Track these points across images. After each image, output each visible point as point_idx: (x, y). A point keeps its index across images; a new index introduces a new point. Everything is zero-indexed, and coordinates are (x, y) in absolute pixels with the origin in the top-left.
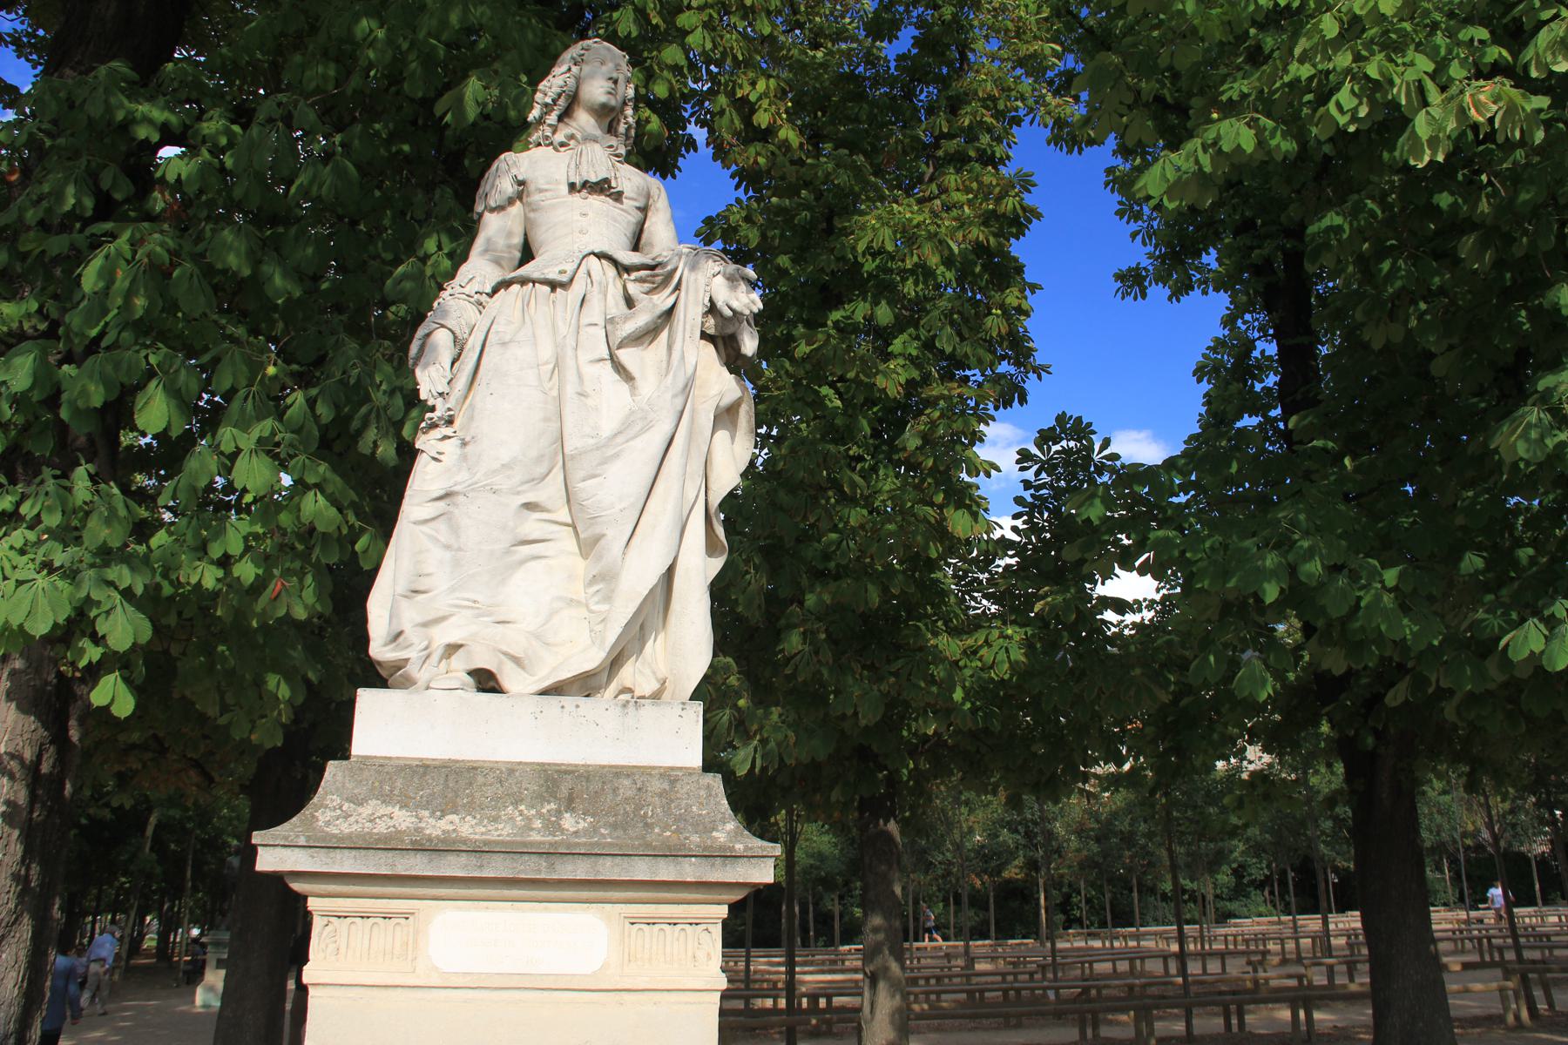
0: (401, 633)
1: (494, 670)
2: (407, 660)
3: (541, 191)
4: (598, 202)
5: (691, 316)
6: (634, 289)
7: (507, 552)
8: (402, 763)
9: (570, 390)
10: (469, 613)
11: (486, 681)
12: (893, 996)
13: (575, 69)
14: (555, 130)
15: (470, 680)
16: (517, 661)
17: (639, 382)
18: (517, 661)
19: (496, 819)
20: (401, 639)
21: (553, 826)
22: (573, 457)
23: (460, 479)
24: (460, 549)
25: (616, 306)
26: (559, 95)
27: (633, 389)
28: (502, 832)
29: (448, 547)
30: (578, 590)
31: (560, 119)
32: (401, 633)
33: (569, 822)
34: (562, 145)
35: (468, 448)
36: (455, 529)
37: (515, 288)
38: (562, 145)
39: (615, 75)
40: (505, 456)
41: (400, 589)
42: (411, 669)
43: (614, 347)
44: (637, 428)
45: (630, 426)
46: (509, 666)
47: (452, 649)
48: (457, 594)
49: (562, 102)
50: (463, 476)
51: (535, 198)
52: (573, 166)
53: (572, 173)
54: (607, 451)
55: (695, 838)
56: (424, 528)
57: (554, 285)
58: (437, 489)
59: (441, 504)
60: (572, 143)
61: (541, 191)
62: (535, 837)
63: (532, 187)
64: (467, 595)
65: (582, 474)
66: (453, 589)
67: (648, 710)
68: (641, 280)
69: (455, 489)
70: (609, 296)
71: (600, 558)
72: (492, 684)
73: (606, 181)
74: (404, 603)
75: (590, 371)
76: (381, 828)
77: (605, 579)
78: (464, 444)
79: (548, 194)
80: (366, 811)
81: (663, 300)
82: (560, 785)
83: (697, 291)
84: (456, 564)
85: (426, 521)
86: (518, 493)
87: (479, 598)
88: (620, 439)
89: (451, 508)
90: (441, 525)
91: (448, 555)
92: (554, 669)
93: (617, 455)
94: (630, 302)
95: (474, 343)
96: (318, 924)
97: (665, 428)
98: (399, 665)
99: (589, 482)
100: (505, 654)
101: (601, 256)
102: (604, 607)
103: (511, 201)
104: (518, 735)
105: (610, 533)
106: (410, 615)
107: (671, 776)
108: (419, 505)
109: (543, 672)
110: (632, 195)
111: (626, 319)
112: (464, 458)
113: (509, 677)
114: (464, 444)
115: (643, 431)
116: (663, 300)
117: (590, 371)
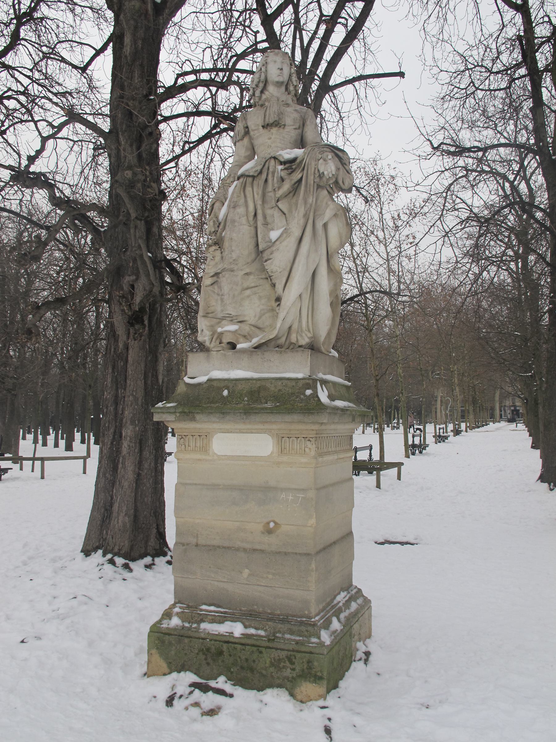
4: (274, 130)
10: (229, 319)
17: (287, 215)
24: (222, 295)
26: (259, 82)
29: (218, 295)
36: (220, 288)
48: (224, 312)
49: (261, 85)
50: (221, 266)
51: (252, 133)
57: (254, 177)
59: (215, 278)
64: (227, 312)
66: (222, 311)
75: (269, 212)
79: (256, 132)
81: (297, 176)
83: (311, 168)
84: (222, 300)
86: (242, 270)
90: (216, 287)
116: (297, 176)
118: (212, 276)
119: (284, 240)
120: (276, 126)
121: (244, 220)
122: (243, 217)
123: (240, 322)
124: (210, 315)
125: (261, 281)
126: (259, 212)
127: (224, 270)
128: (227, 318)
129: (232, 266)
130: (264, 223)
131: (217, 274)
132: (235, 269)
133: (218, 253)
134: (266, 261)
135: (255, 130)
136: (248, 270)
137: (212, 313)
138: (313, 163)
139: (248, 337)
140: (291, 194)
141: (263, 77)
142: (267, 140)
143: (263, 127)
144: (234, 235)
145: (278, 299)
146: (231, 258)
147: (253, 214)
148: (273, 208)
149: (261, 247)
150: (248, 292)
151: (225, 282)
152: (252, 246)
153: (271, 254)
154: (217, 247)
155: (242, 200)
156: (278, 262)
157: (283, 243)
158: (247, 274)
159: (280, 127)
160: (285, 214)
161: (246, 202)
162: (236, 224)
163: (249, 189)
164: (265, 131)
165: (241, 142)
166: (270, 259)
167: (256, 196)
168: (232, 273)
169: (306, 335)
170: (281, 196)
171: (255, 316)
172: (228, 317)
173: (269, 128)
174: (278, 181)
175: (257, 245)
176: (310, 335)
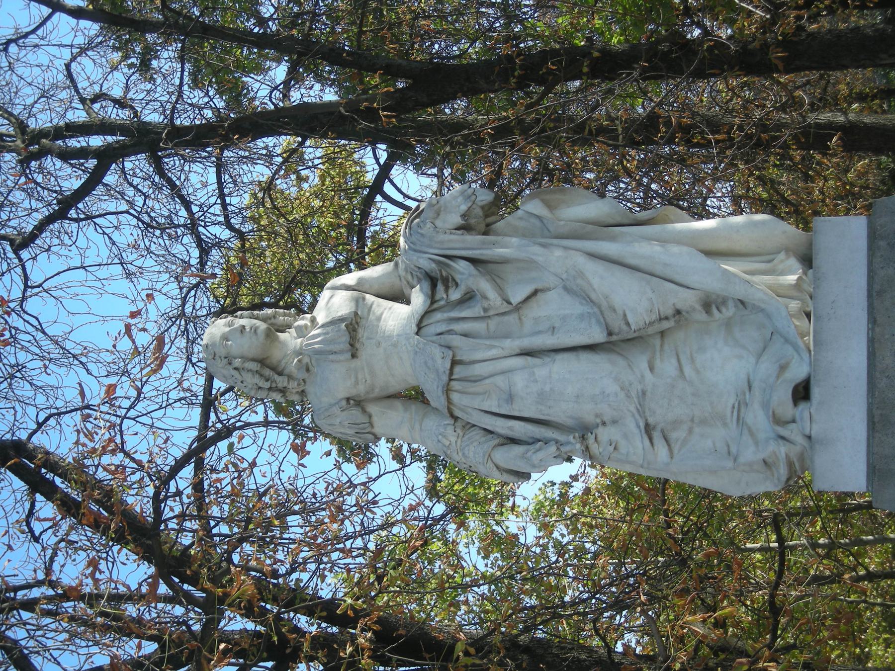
0: (765, 462)
1: (793, 385)
2: (787, 455)
5: (472, 244)
10: (743, 410)
11: (802, 392)
12: (571, 417)
14: (290, 377)
17: (539, 286)
18: (783, 368)
20: (770, 461)
22: (610, 334)
23: (632, 426)
24: (692, 420)
26: (261, 375)
29: (690, 431)
31: (280, 374)
32: (765, 462)
36: (676, 423)
37: (455, 397)
38: (308, 370)
42: (794, 451)
43: (509, 308)
48: (728, 421)
49: (267, 372)
56: (675, 451)
57: (454, 363)
58: (639, 443)
59: (656, 435)
61: (357, 383)
63: (353, 392)
65: (625, 327)
66: (725, 425)
69: (642, 425)
72: (801, 389)
74: (742, 460)
79: (360, 376)
83: (450, 241)
84: (703, 422)
86: (643, 376)
87: (730, 405)
88: (593, 296)
89: (659, 428)
90: (673, 435)
91: (697, 430)
94: (469, 298)
95: (502, 426)
97: (581, 261)
98: (790, 465)
100: (778, 377)
102: (731, 304)
103: (364, 411)
106: (750, 454)
107: (873, 236)
111: (485, 297)
112: (614, 422)
115: (581, 274)
117: (528, 325)
118: (651, 439)
119: (590, 285)
120: (355, 330)
122: (534, 373)
123: (750, 387)
124: (734, 450)
125: (666, 347)
127: (641, 411)
128: (742, 415)
129: (633, 394)
130: (550, 333)
131: (648, 430)
132: (639, 388)
133: (602, 432)
134: (628, 324)
135: (357, 378)
136: (644, 365)
137: (728, 446)
138: (442, 237)
139: (783, 361)
140: (498, 281)
141: (254, 366)
143: (354, 356)
145: (709, 304)
146: (616, 394)
147: (529, 358)
148: (520, 319)
149: (598, 336)
150: (688, 370)
153: (614, 310)
154: (591, 439)
155: (500, 381)
156: (633, 301)
157: (596, 286)
158: (652, 369)
159: (357, 323)
160: (535, 293)
161: (503, 372)
162: (547, 388)
163: (479, 370)
164: (363, 354)
165: (375, 419)
166: (625, 315)
167: (493, 353)
168: (648, 394)
169: (782, 261)
170: (500, 295)
171: (740, 357)
172: (739, 411)
173: (357, 345)
174: (469, 307)
175: (591, 348)
176: (782, 256)
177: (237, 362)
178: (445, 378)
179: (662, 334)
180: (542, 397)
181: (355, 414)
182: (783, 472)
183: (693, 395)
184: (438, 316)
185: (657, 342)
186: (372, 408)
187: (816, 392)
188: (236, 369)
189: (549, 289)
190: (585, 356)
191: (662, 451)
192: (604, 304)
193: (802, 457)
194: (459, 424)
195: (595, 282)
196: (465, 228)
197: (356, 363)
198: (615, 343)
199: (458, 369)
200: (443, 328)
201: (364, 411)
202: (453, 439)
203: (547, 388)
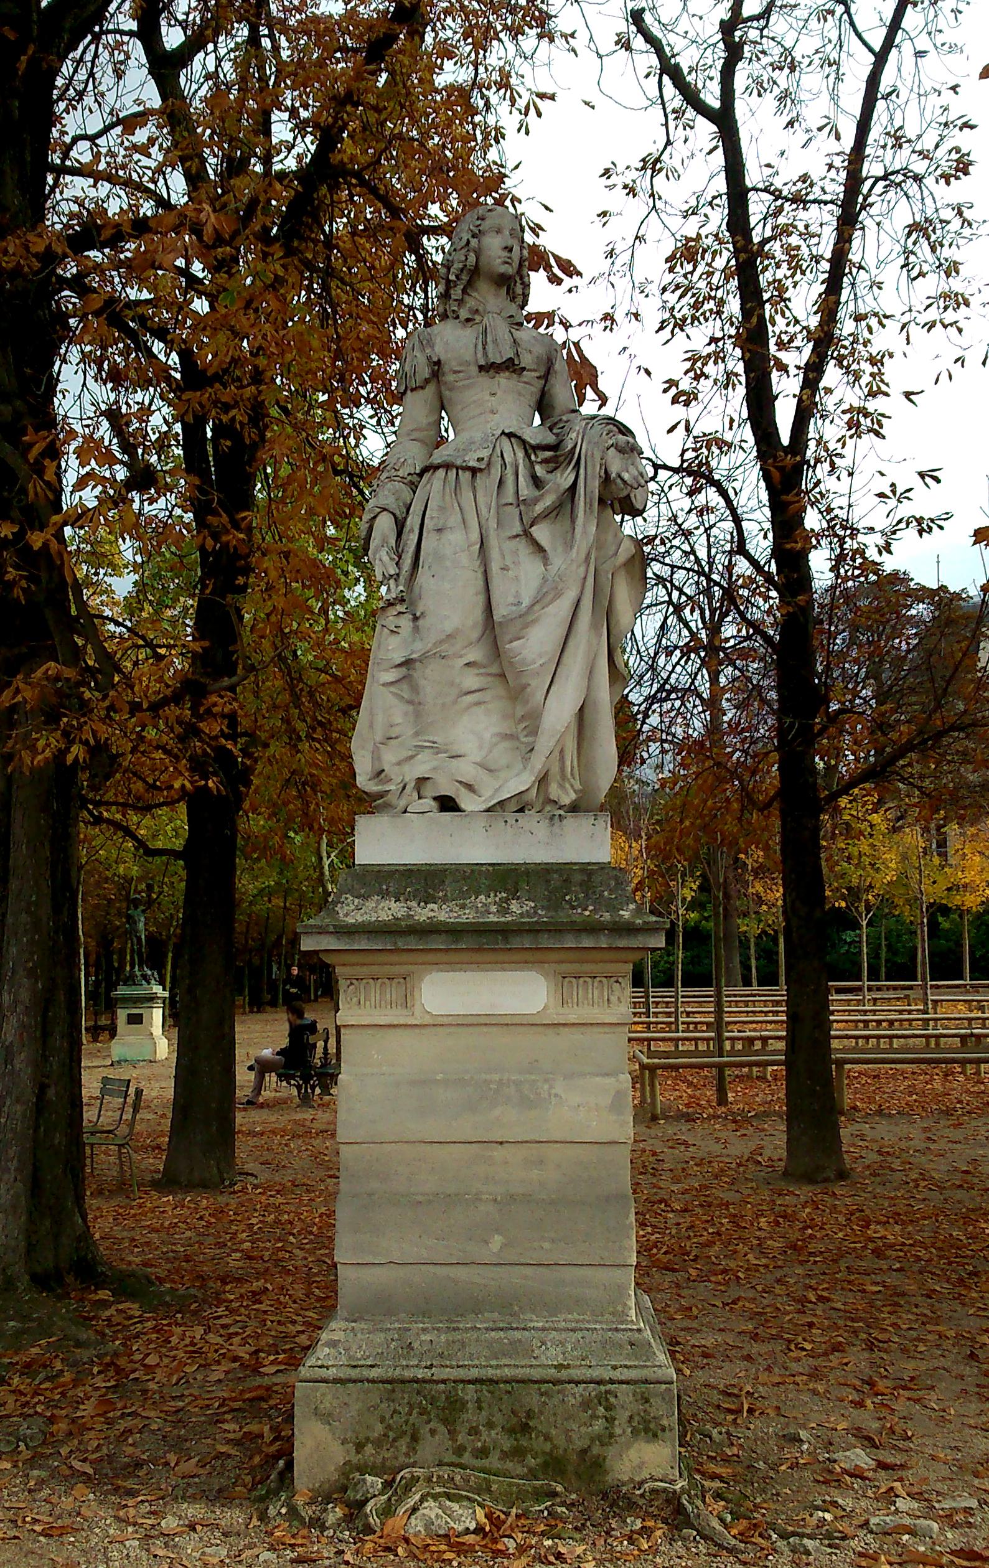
3: (455, 372)
4: (503, 380)
6: (539, 470)
7: (455, 702)
8: (377, 869)
9: (495, 567)
11: (447, 804)
13: (474, 242)
14: (460, 302)
15: (433, 803)
16: (470, 787)
18: (470, 787)
19: (463, 907)
21: (504, 911)
23: (418, 648)
25: (526, 490)
26: (462, 270)
27: (546, 561)
28: (468, 916)
29: (410, 702)
30: (506, 727)
31: (464, 291)
33: (514, 906)
34: (468, 320)
35: (420, 622)
36: (415, 689)
37: (441, 472)
39: (509, 244)
40: (449, 627)
41: (379, 737)
42: (391, 798)
44: (550, 596)
45: (545, 596)
46: (463, 790)
47: (421, 781)
49: (465, 277)
51: (450, 378)
52: (480, 347)
53: (480, 355)
54: (526, 618)
55: (607, 916)
56: (392, 689)
57: (474, 471)
59: (403, 670)
60: (478, 318)
61: (455, 372)
62: (493, 918)
63: (446, 368)
65: (508, 638)
66: (417, 734)
67: (570, 822)
68: (545, 461)
69: (414, 656)
70: (521, 478)
71: (527, 702)
73: (511, 360)
76: (384, 916)
77: (532, 722)
78: (416, 618)
80: (371, 904)
81: (565, 478)
82: (506, 878)
83: (594, 466)
84: (418, 715)
85: (392, 683)
88: (537, 607)
90: (405, 686)
91: (411, 708)
92: (497, 790)
93: (534, 621)
94: (537, 482)
95: (413, 521)
96: (342, 984)
97: (571, 595)
98: (381, 795)
99: (515, 644)
101: (510, 435)
102: (531, 739)
103: (427, 381)
104: (474, 845)
105: (534, 683)
106: (389, 758)
108: (386, 670)
109: (487, 793)
110: (534, 367)
111: (536, 500)
112: (416, 629)
113: (467, 802)
114: (416, 618)
115: (558, 595)
116: (565, 478)
120: (507, 368)
121: (464, 559)
125: (490, 679)
126: (493, 542)
131: (407, 663)
133: (405, 622)
136: (471, 658)
142: (488, 397)
143: (481, 368)
144: (447, 585)
150: (469, 698)
151: (429, 677)
152: (478, 614)
155: (454, 519)
156: (534, 646)
162: (448, 563)
163: (467, 495)
164: (484, 380)
165: (421, 392)
173: (492, 372)
177: (474, 242)
178: (459, 462)
179: (502, 676)
180: (439, 558)
181: (426, 372)
182: (372, 787)
183: (443, 705)
184: (520, 454)
185: (494, 669)
186: (431, 389)
187: (448, 816)
188: (468, 242)
189: (545, 565)
190: (481, 599)
191: (391, 676)
192: (530, 618)
193: (388, 806)
194: (415, 478)
195: (551, 609)
196: (607, 479)
197: (474, 370)
198: (491, 628)
199: (465, 476)
200: (508, 458)
201: (427, 381)
202: (400, 473)
203: (448, 563)
